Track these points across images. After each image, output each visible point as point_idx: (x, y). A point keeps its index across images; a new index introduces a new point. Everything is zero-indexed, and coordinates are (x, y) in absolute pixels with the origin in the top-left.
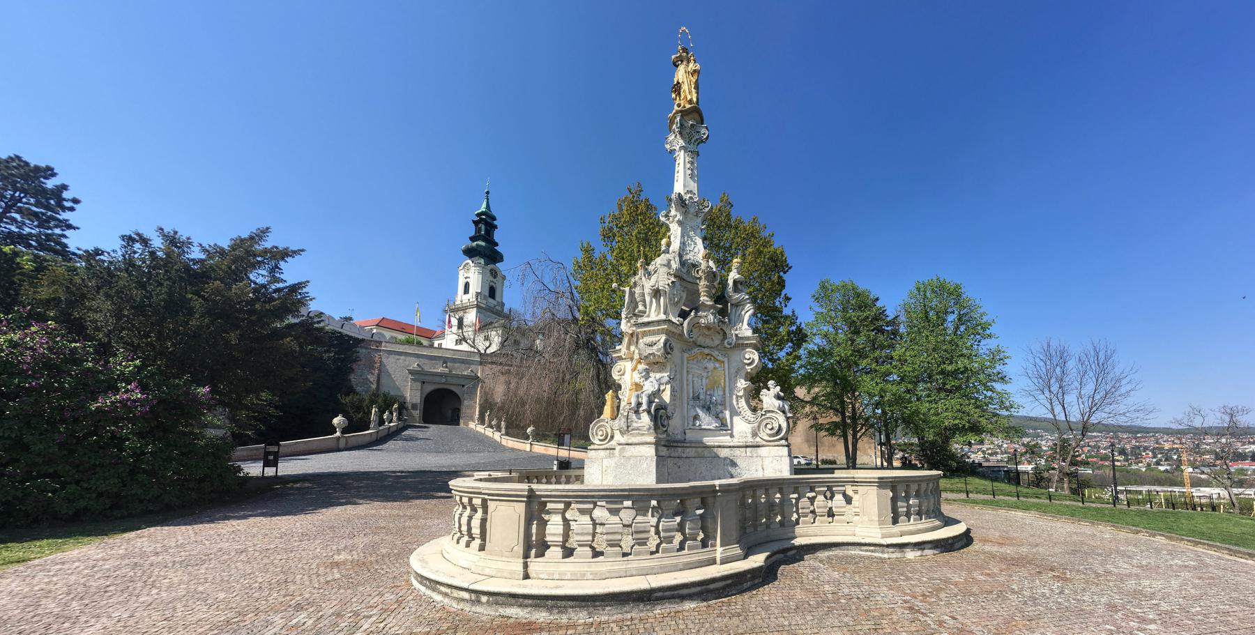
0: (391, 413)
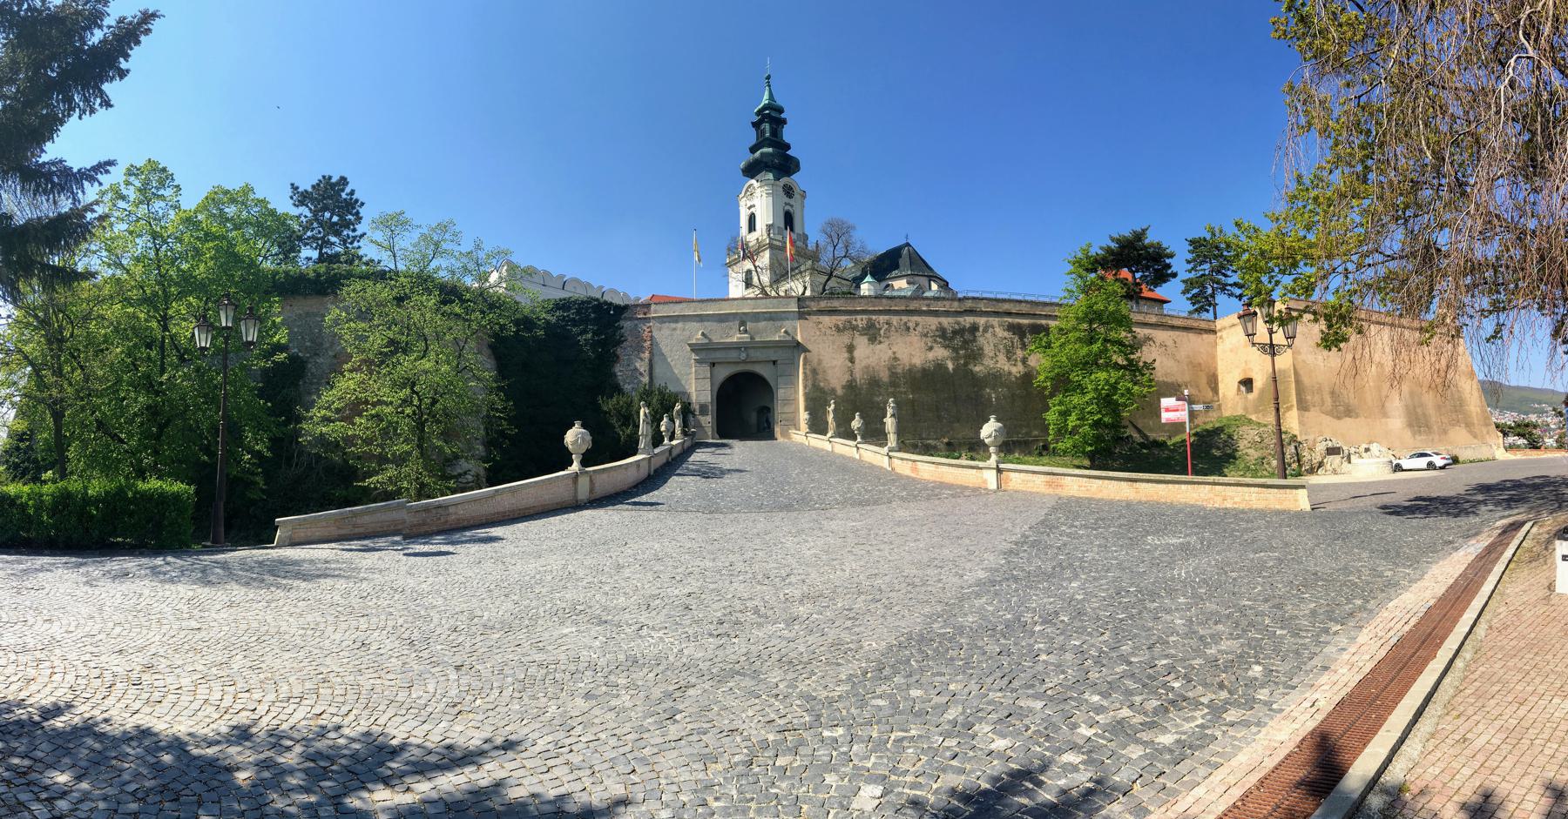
0: (672, 420)
